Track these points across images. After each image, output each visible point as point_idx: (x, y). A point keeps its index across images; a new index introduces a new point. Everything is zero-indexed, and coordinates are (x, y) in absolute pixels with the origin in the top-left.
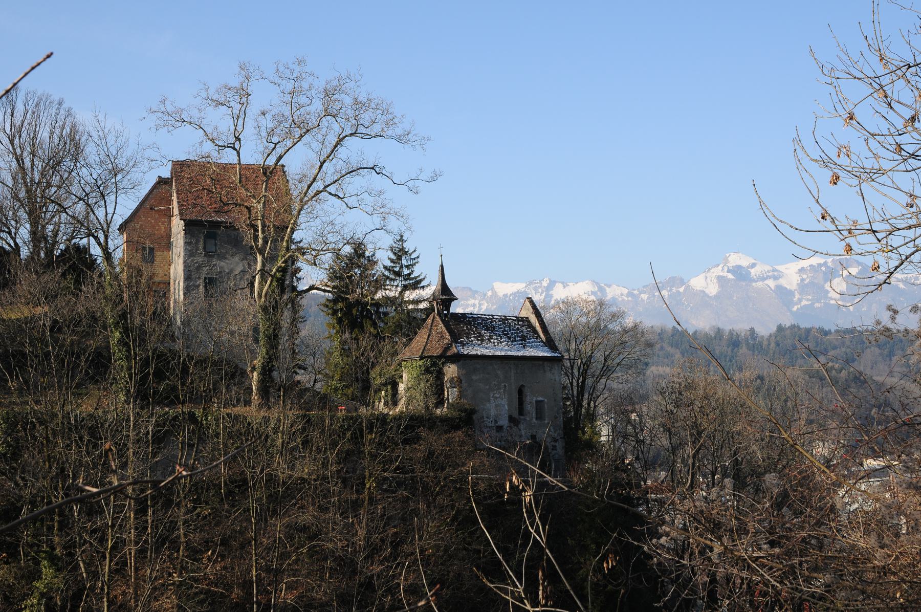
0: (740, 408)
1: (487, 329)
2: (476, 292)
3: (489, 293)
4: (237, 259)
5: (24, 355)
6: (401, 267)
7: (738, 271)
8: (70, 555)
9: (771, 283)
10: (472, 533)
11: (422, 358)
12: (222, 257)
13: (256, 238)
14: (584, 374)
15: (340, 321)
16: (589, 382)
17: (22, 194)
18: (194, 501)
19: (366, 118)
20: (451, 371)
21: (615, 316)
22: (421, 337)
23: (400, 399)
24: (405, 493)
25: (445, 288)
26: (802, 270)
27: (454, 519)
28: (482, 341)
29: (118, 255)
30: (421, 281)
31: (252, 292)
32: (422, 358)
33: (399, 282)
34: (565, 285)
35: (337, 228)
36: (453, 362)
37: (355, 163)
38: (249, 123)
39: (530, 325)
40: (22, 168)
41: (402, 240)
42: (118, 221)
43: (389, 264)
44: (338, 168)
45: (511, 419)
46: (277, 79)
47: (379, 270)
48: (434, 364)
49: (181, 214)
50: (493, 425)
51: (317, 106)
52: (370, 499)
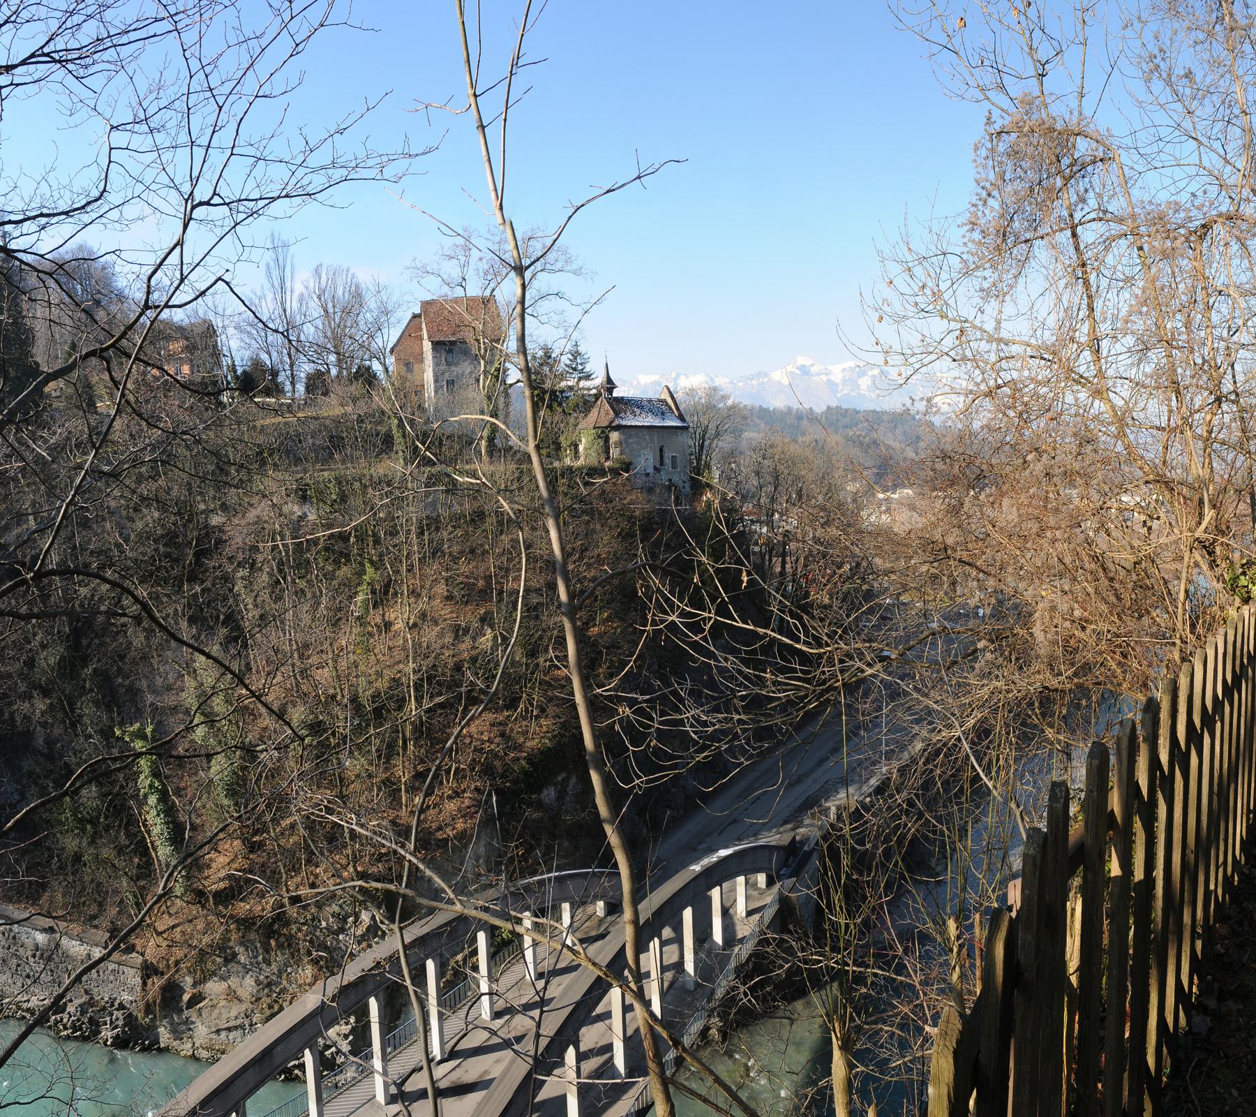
0: (805, 461)
4: (466, 364)
7: (804, 370)
8: (381, 560)
9: (824, 377)
10: (632, 543)
12: (456, 365)
14: (703, 438)
16: (707, 443)
17: (329, 334)
18: (454, 527)
20: (614, 436)
21: (724, 398)
24: (587, 518)
25: (609, 380)
26: (844, 370)
27: (620, 534)
29: (391, 369)
33: (576, 375)
34: (687, 376)
35: (535, 338)
37: (544, 291)
38: (472, 266)
39: (667, 405)
40: (326, 311)
41: (576, 345)
42: (390, 345)
44: (533, 295)
45: (655, 468)
46: (489, 236)
47: (561, 367)
49: (429, 338)
52: (564, 522)
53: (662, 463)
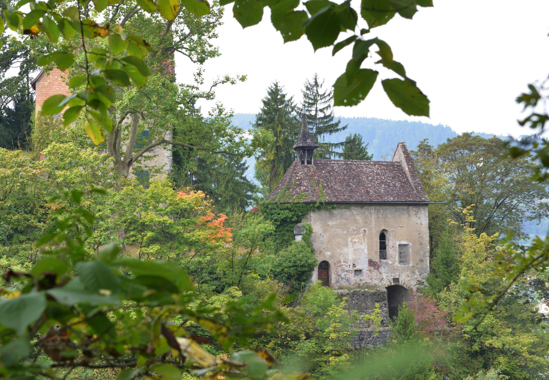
6: (316, 111)
45: (371, 263)
50: (351, 268)
53: (383, 254)
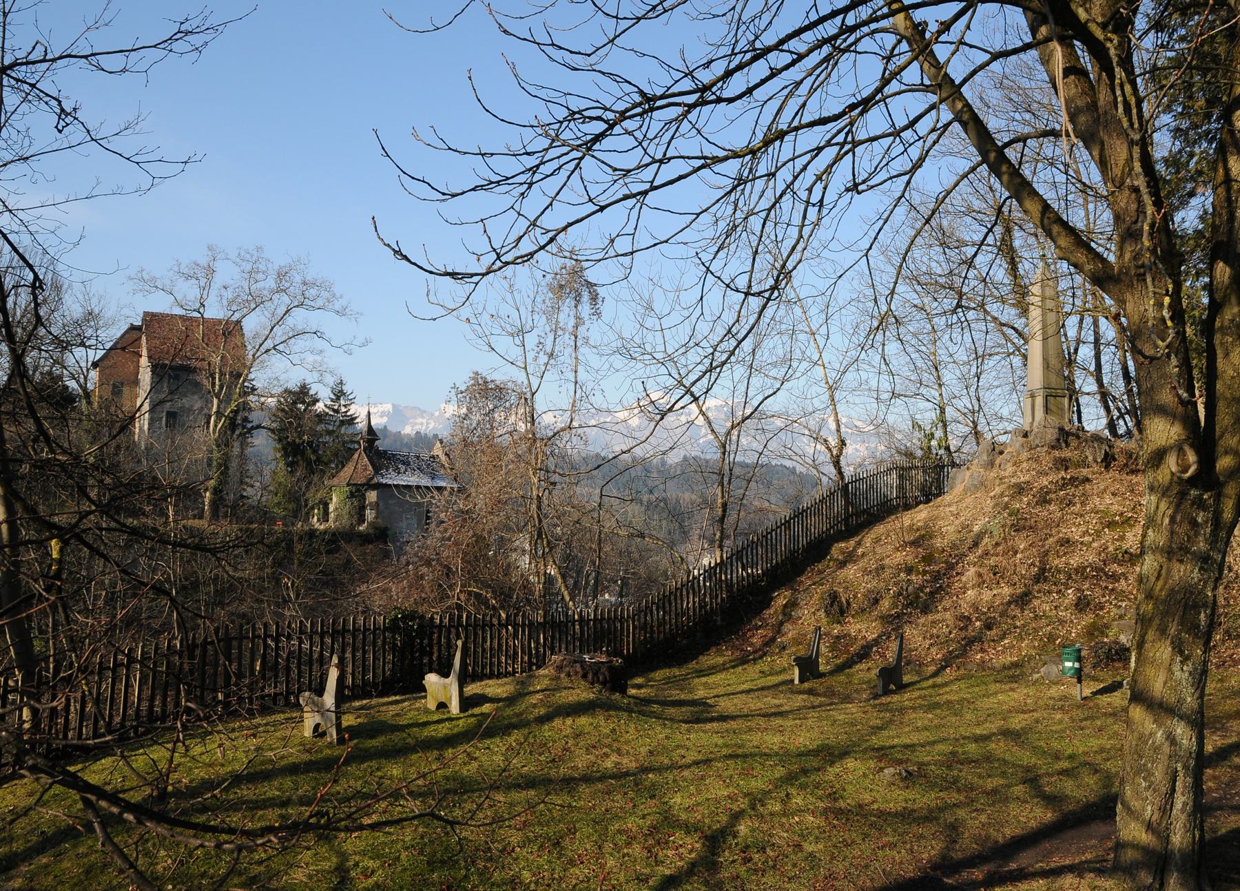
1: (404, 464)
2: (425, 412)
3: (437, 414)
4: (196, 397)
5: (525, 822)
11: (348, 485)
13: (213, 384)
15: (284, 449)
19: (312, 292)
20: (372, 496)
22: (348, 471)
23: (990, 174)
28: (399, 473)
30: (356, 418)
31: (208, 427)
32: (348, 485)
36: (373, 490)
37: (300, 328)
38: (213, 292)
41: (341, 383)
43: (329, 403)
48: (358, 490)
51: (271, 283)
